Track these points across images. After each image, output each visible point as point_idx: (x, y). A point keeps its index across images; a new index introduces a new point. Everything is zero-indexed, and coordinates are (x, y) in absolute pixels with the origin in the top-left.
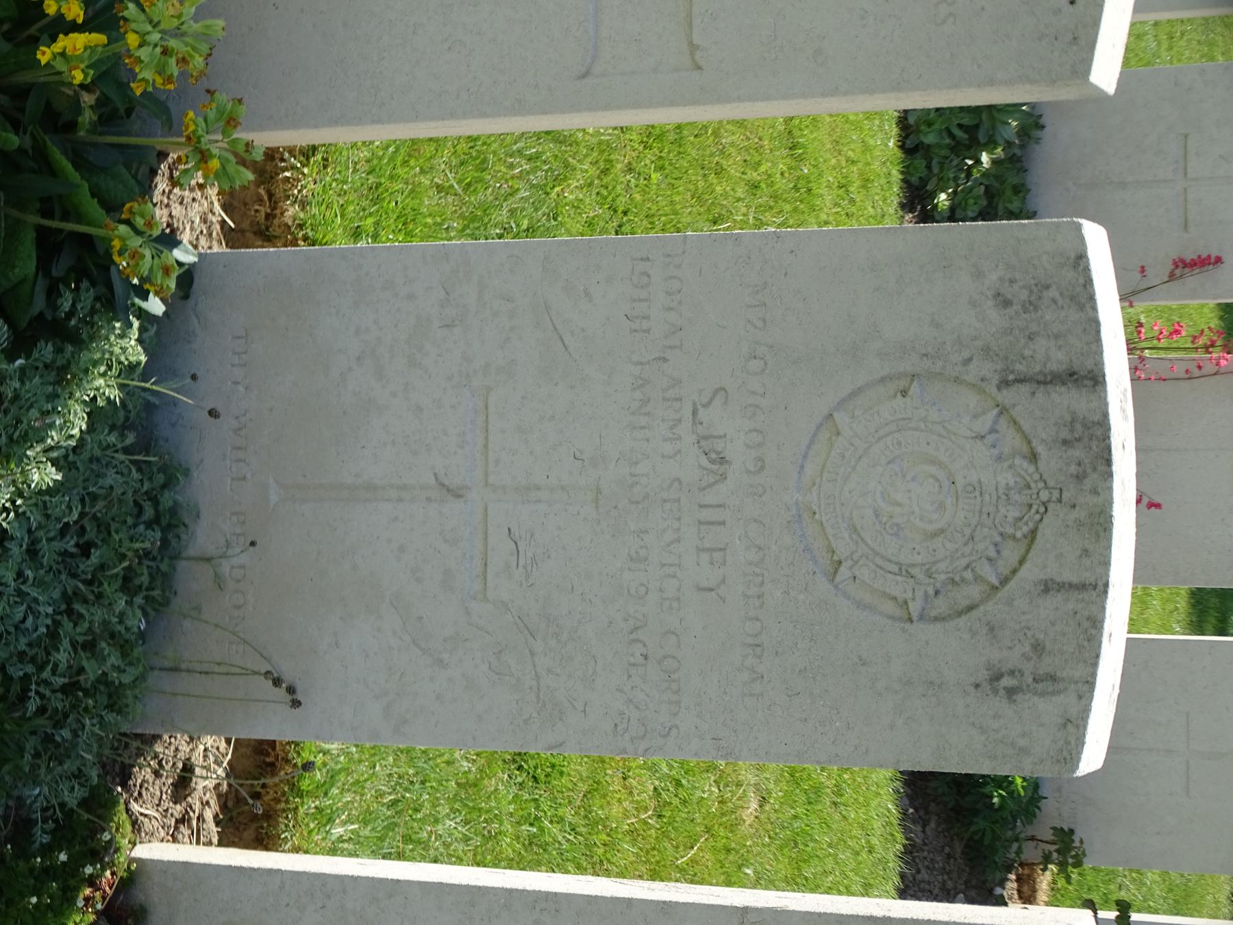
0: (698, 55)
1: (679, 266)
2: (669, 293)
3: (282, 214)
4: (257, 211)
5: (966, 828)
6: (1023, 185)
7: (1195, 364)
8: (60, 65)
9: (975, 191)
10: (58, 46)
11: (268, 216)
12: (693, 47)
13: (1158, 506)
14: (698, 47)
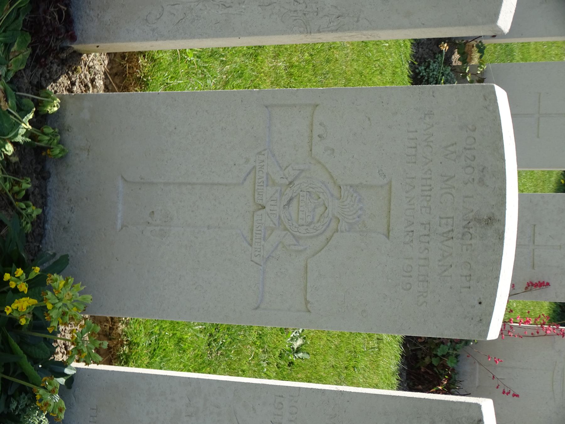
0: (309, 306)
1: (296, 402)
2: (291, 414)
3: (117, 328)
4: (105, 326)
7: (536, 331)
8: (15, 315)
10: (14, 306)
11: (110, 328)
12: (307, 302)
13: (517, 396)
14: (309, 302)
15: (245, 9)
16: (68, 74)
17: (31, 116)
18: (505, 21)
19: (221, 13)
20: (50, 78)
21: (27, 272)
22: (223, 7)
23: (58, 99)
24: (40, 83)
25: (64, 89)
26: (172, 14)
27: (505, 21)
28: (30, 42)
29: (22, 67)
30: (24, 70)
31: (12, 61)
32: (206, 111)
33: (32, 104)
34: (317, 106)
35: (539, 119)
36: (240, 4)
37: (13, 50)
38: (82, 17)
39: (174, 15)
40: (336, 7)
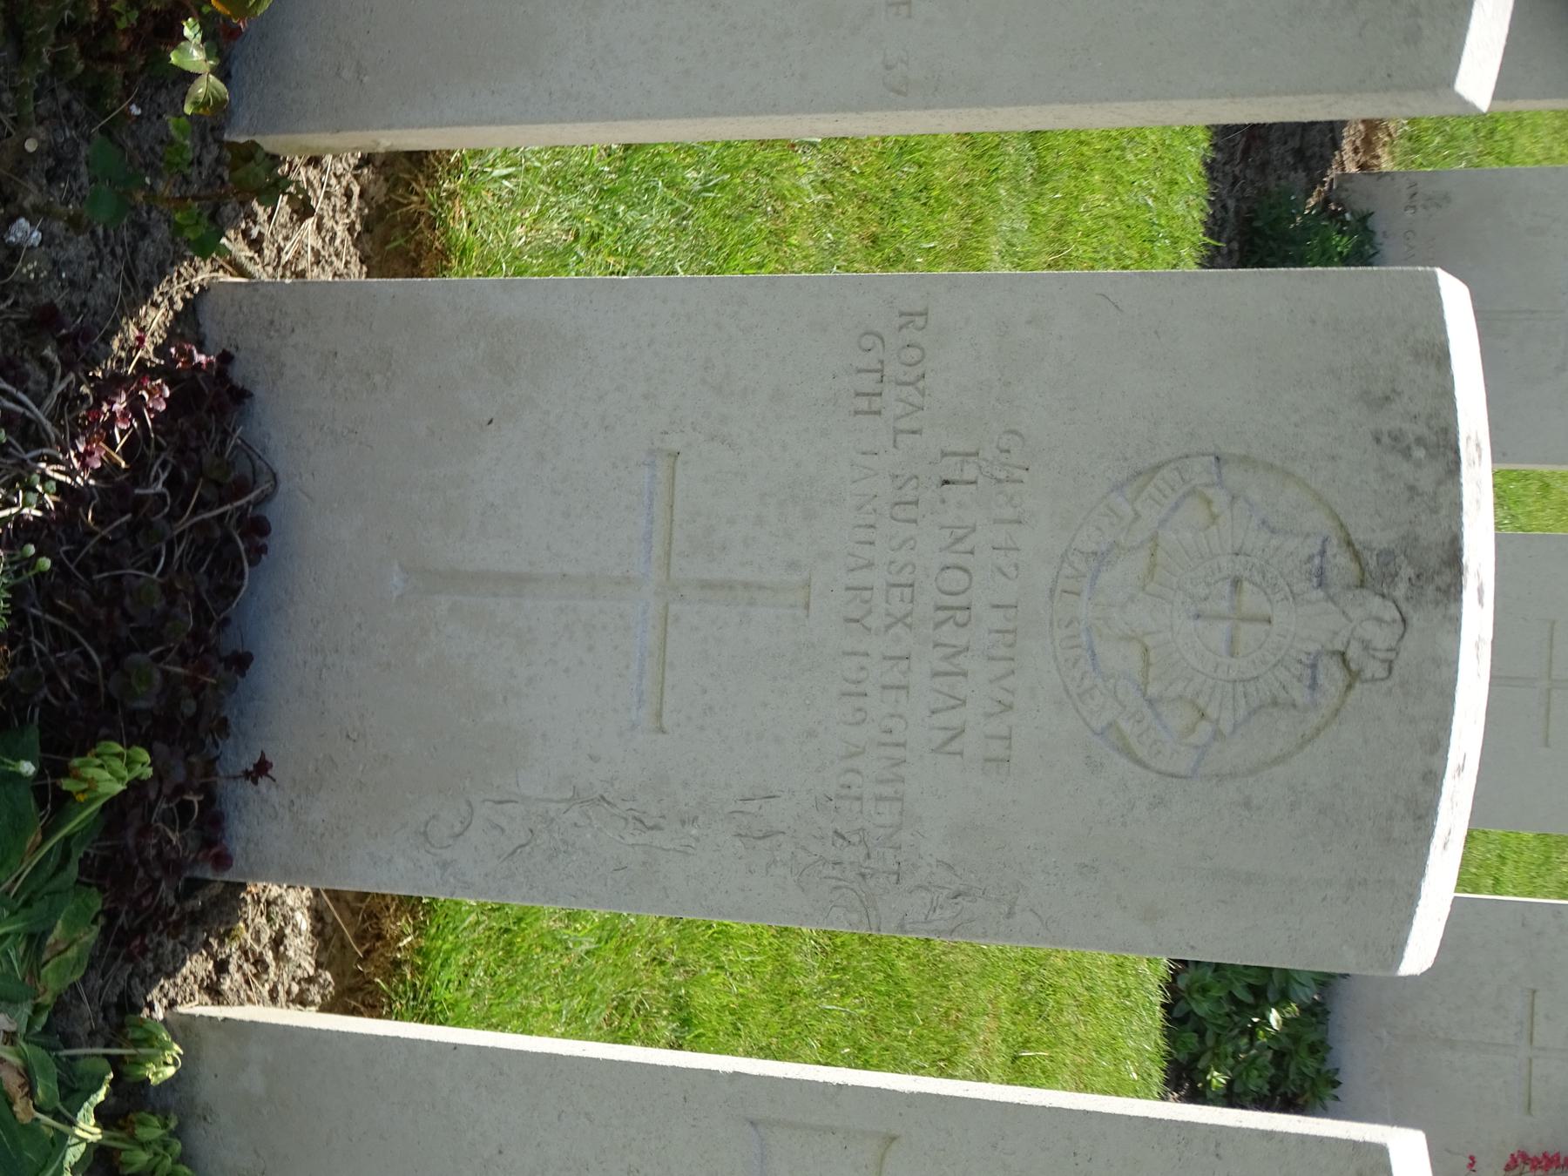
5: (1252, 1033)
6: (1322, 1042)
9: (1260, 1061)
15: (697, 840)
16: (207, 945)
17: (101, 1096)
18: (1477, 76)
19: (630, 840)
20: (158, 970)
21: (236, 228)
22: (639, 825)
23: (176, 1047)
24: (129, 998)
25: (196, 987)
26: (496, 826)
27: (1477, 76)
28: (99, 907)
29: (76, 977)
30: (84, 980)
31: (49, 966)
32: (587, 1115)
33: (105, 1064)
34: (893, 1139)
35: (1549, 690)
36: (683, 823)
37: (51, 940)
38: (246, 804)
39: (503, 830)
40: (950, 867)
